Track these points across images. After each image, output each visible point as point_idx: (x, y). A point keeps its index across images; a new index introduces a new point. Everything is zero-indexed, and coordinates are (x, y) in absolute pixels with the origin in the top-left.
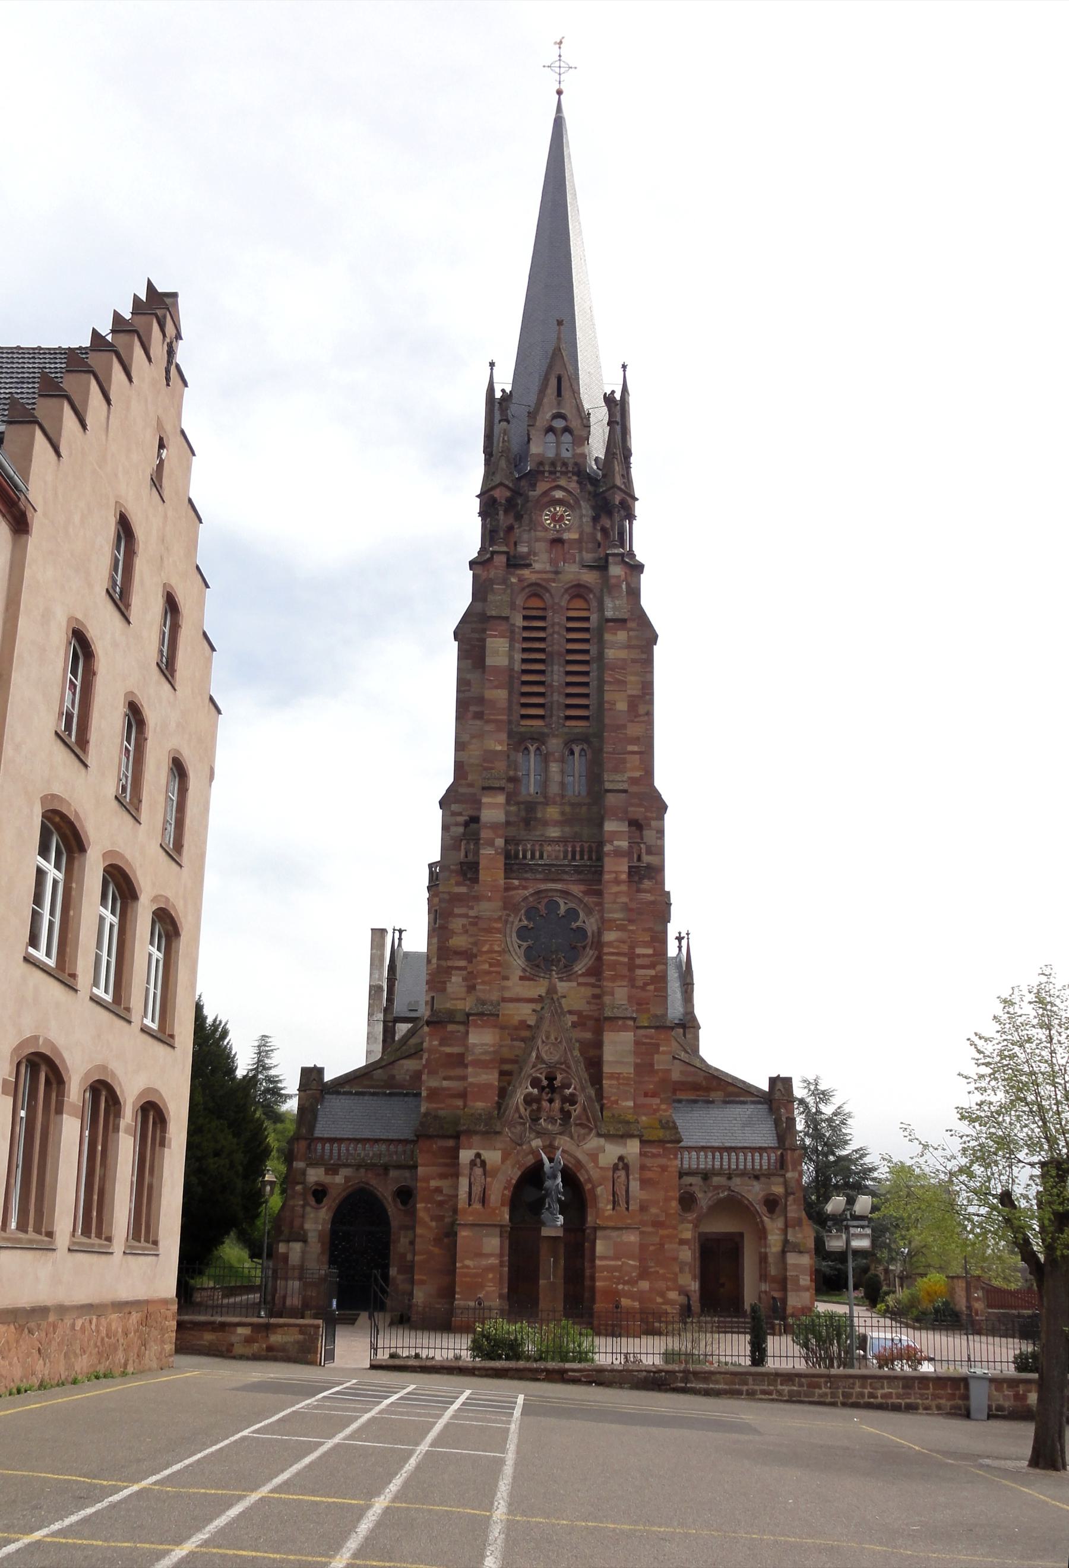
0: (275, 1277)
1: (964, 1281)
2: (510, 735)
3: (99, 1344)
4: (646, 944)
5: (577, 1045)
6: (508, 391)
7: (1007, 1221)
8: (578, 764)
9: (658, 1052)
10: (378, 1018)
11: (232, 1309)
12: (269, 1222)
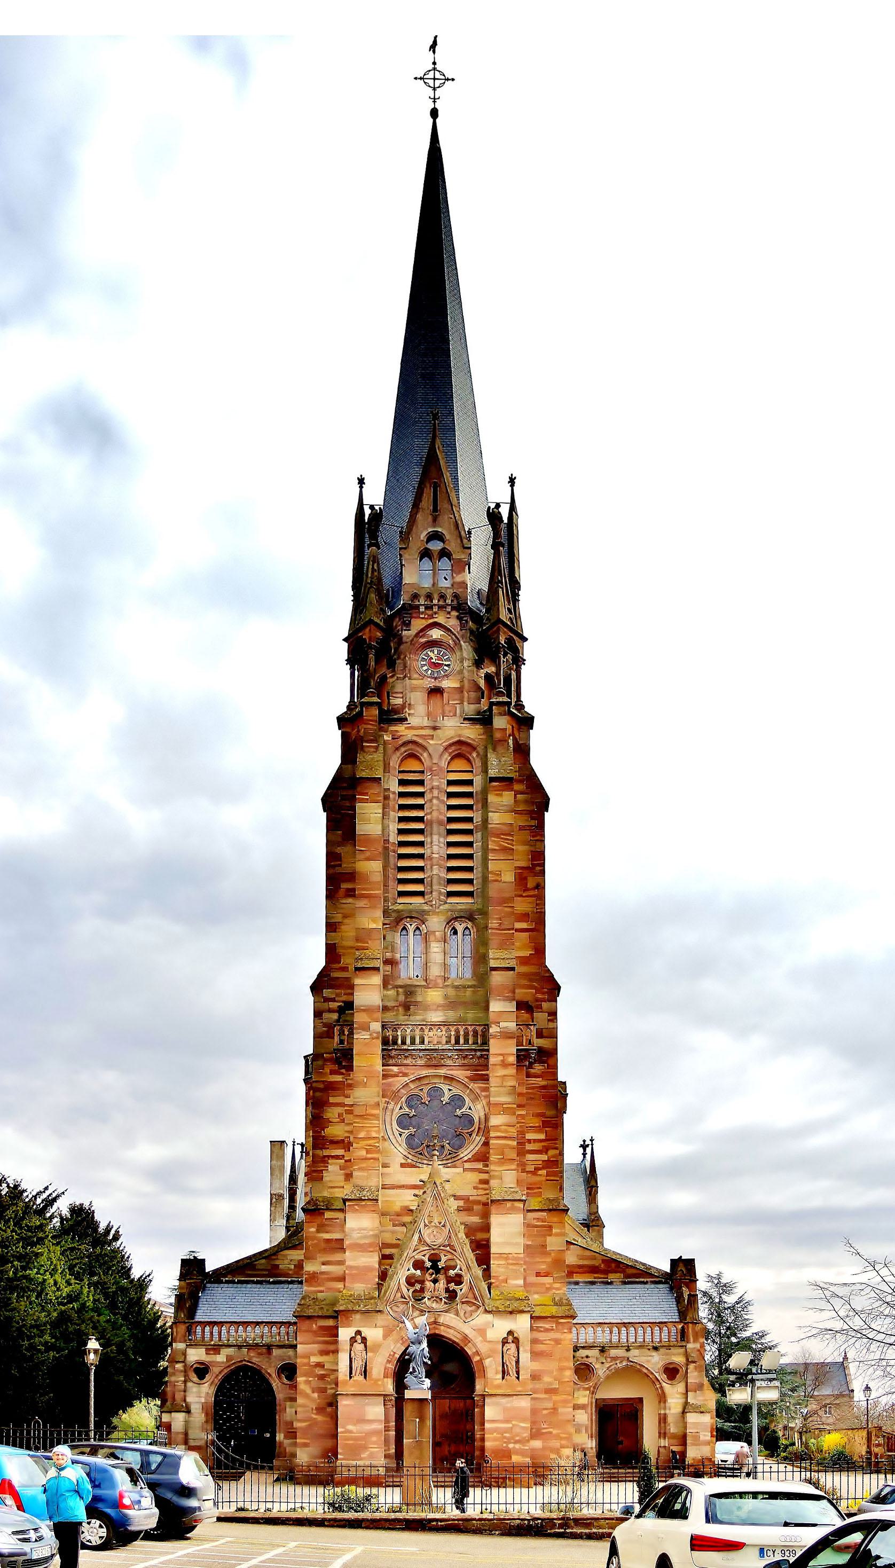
2: (386, 913)
8: (463, 944)
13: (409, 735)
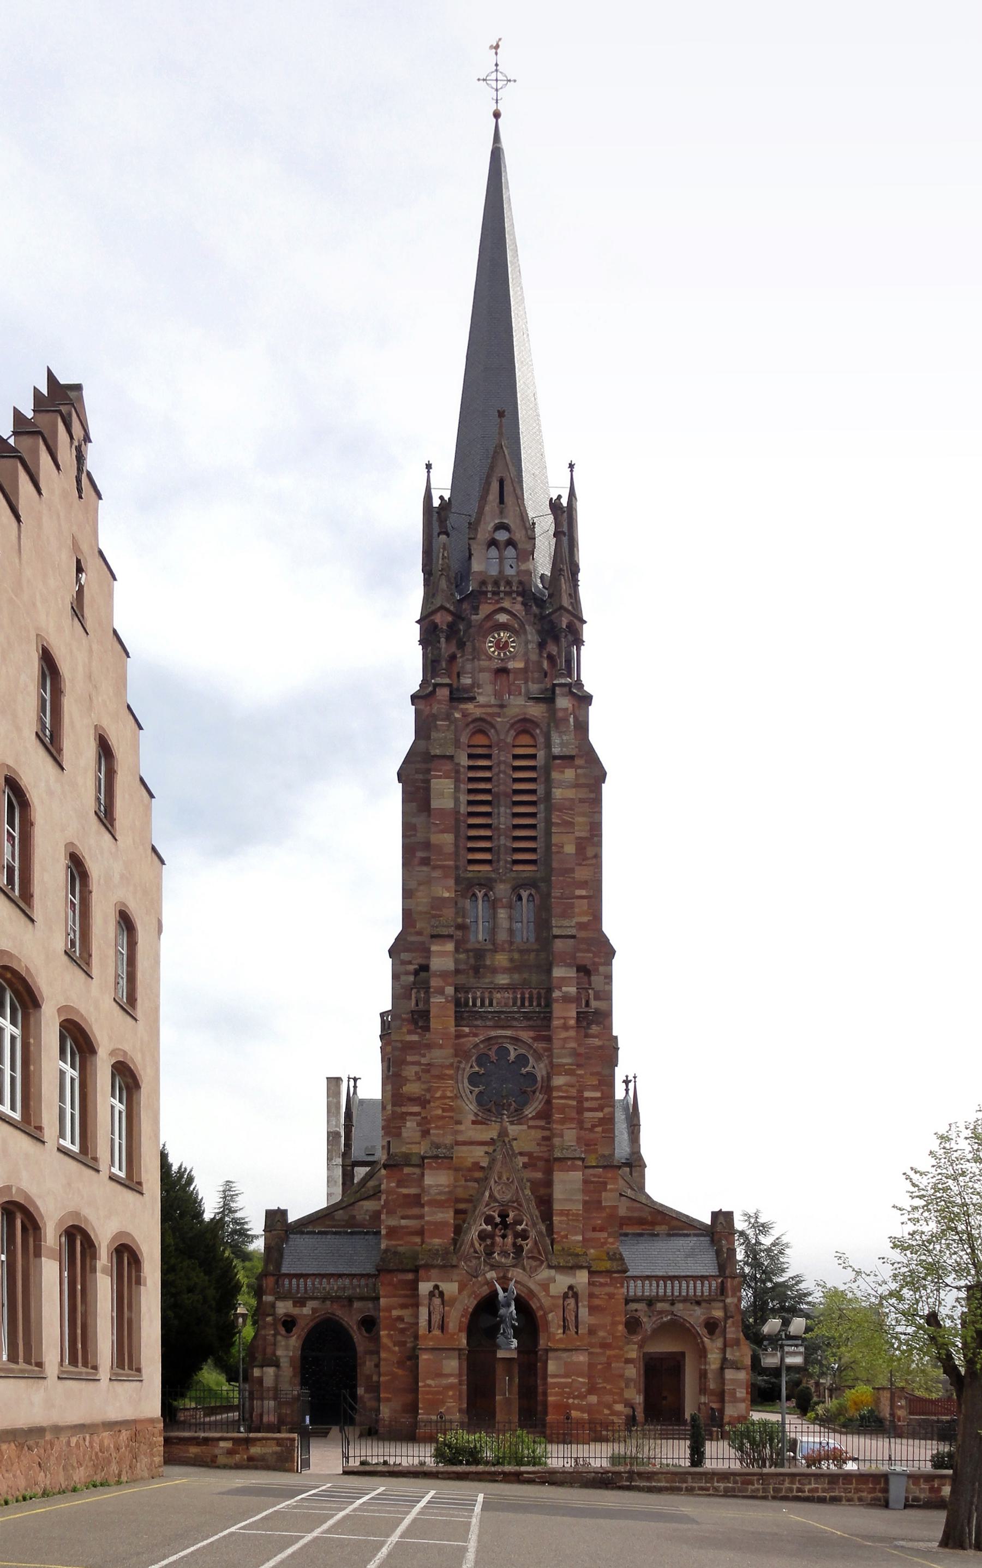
0: (252, 1398)
1: (889, 1392)
2: (458, 881)
3: (94, 1458)
4: (594, 1088)
5: (528, 1184)
6: (446, 498)
7: (932, 1339)
8: (526, 909)
9: (605, 1190)
12: (243, 1350)
13: (478, 712)
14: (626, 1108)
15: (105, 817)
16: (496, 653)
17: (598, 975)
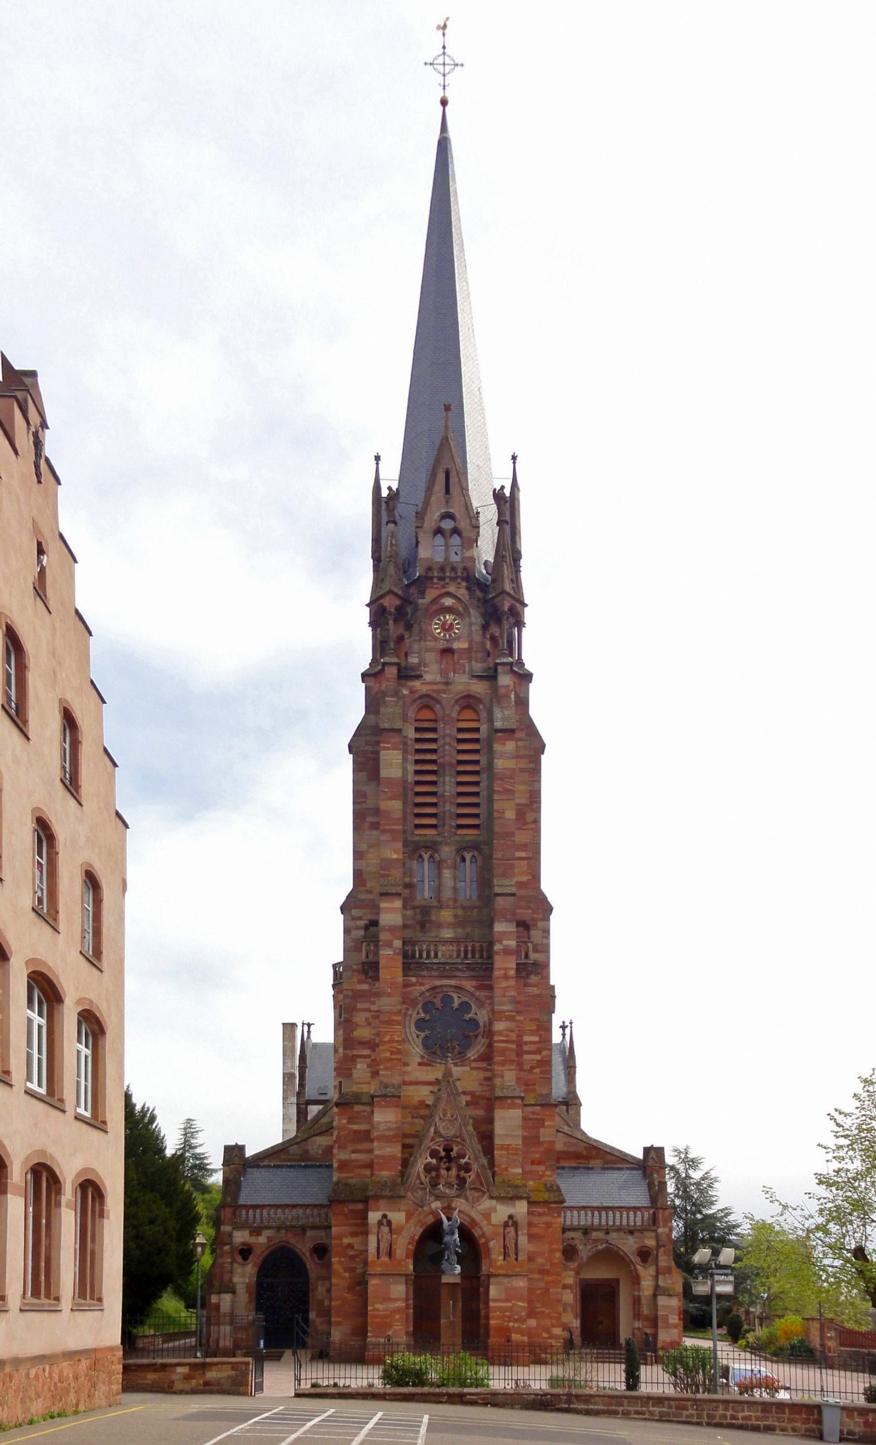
0: (209, 1324)
1: (818, 1323)
2: (406, 843)
3: (52, 1388)
4: (533, 1033)
5: (471, 1121)
6: (394, 488)
7: (860, 1272)
8: (469, 870)
9: (543, 1126)
10: (292, 1101)
11: (173, 1352)
12: (202, 1277)
13: (424, 689)
14: (563, 1051)
15: (71, 784)
16: (442, 634)
17: (537, 929)
